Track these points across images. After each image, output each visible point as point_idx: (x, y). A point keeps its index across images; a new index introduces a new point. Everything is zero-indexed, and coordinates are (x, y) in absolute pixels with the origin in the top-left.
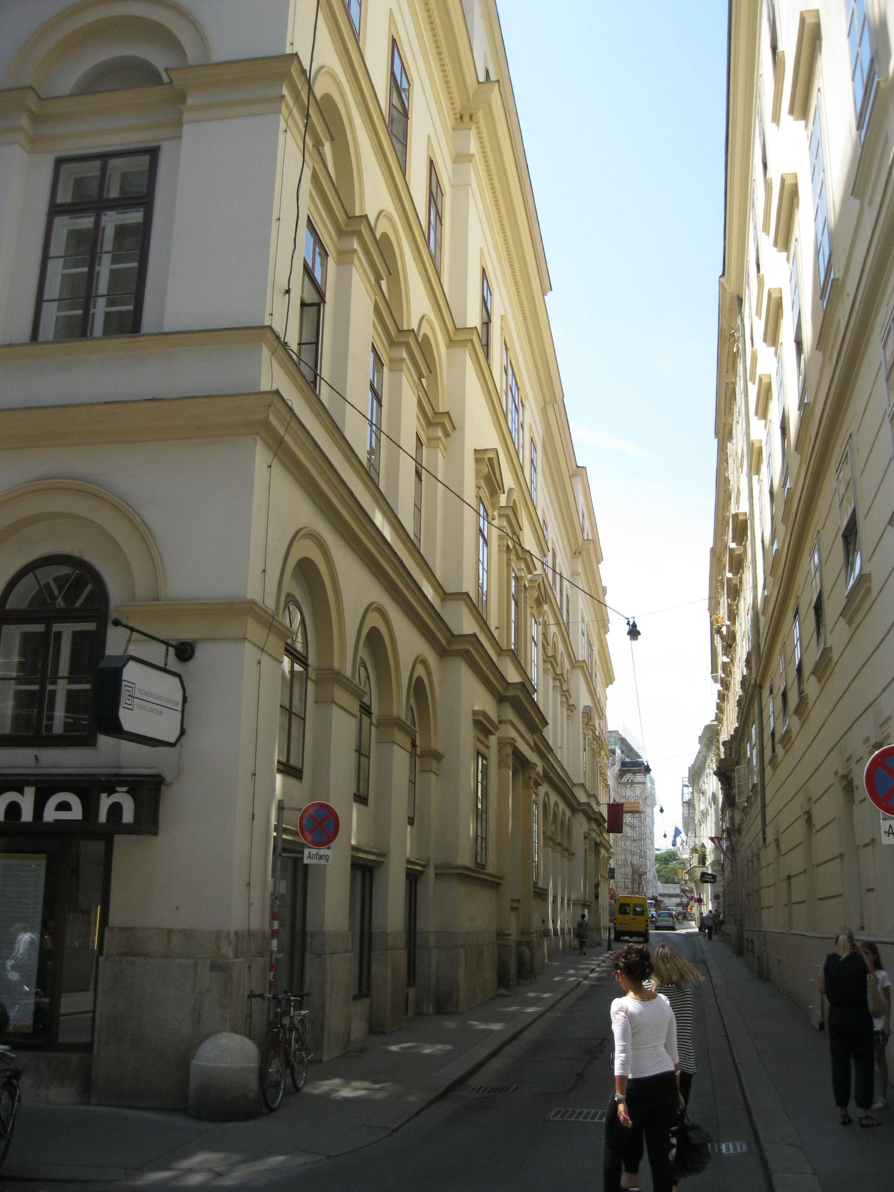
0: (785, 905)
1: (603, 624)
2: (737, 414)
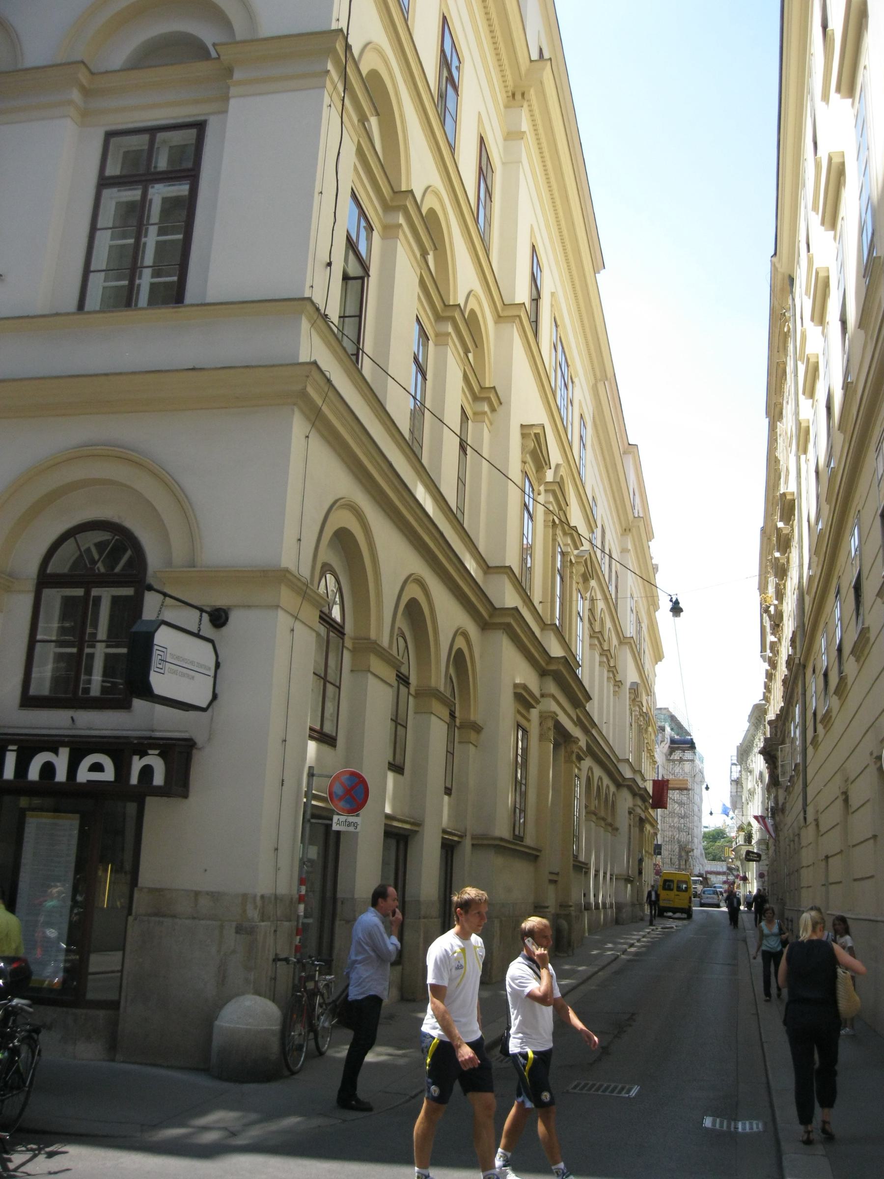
0: (823, 885)
1: (653, 603)
2: (788, 394)
